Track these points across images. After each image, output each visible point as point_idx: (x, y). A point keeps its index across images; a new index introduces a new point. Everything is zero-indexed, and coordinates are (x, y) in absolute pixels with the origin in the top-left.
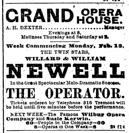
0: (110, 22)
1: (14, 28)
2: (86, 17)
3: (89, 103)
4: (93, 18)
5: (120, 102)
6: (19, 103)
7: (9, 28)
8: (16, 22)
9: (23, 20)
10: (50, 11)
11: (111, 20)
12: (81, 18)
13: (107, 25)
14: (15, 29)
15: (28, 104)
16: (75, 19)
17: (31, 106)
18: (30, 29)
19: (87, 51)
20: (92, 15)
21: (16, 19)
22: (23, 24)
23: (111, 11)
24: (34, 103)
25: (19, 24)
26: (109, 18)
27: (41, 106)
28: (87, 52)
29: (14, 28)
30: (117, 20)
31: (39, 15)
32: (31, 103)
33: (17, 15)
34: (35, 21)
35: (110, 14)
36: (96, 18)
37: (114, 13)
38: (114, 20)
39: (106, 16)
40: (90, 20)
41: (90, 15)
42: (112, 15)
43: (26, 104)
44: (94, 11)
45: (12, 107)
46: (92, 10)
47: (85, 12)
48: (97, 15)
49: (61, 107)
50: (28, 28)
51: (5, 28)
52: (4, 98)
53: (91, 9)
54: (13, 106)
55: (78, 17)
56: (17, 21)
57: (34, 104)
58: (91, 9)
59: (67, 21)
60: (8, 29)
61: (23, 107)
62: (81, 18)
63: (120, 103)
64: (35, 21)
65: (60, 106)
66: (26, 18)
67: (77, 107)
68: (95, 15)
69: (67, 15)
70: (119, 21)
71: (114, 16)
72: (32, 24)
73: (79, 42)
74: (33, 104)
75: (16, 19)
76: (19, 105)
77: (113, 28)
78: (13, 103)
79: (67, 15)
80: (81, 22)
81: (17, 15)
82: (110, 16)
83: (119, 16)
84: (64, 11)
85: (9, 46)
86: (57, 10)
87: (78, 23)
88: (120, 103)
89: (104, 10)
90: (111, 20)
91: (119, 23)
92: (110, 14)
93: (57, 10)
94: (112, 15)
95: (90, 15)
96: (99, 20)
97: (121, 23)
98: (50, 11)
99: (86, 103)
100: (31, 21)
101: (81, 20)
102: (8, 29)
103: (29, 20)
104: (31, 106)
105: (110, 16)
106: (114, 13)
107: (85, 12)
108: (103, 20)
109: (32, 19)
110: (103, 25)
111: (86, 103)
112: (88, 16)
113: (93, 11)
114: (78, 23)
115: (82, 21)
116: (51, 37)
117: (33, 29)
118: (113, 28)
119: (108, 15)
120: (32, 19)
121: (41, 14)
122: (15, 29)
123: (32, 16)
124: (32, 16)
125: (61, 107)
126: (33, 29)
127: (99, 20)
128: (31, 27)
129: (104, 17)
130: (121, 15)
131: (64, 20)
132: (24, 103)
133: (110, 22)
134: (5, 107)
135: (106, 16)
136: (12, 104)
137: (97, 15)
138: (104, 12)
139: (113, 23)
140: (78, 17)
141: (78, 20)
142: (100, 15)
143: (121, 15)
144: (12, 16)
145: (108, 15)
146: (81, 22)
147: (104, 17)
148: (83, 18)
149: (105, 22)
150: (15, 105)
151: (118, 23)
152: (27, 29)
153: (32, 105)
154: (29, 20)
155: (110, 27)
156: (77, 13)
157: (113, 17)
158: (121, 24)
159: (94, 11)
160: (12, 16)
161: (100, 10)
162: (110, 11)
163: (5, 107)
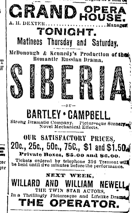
0: (112, 19)
1: (18, 23)
2: (88, 14)
3: (93, 162)
4: (95, 16)
5: (123, 162)
6: (24, 161)
7: (12, 23)
8: (20, 17)
9: (26, 17)
10: (53, 7)
11: (114, 17)
12: (84, 15)
13: (109, 22)
14: (19, 24)
15: (33, 162)
16: (78, 16)
17: (36, 164)
18: (33, 25)
19: (102, 191)
20: (95, 12)
21: (20, 15)
22: (26, 20)
23: (30, 8)
24: (39, 161)
25: (23, 19)
26: (112, 16)
27: (45, 164)
28: (103, 192)
29: (18, 24)
30: (120, 18)
31: (42, 12)
32: (36, 161)
33: (20, 11)
34: (38, 17)
35: (113, 12)
36: (99, 15)
37: (117, 11)
38: (117, 18)
39: (109, 13)
40: (93, 17)
41: (93, 12)
42: (115, 12)
43: (31, 162)
44: (97, 8)
45: (17, 164)
46: (95, 7)
47: (89, 9)
48: (100, 12)
49: (64, 165)
50: (31, 23)
51: (8, 23)
52: (9, 138)
53: (94, 7)
54: (19, 163)
55: (81, 14)
56: (21, 17)
57: (39, 162)
58: (94, 7)
59: (69, 17)
60: (12, 24)
61: (28, 165)
62: (84, 15)
63: (123, 163)
64: (38, 17)
65: (63, 164)
66: (29, 14)
67: (79, 166)
68: (97, 13)
69: (70, 12)
70: (122, 18)
71: (117, 14)
72: (35, 20)
73: (83, 132)
74: (38, 162)
75: (20, 15)
76: (24, 162)
77: (115, 26)
78: (18, 161)
79: (70, 12)
80: (83, 19)
81: (20, 11)
82: (113, 13)
83: (121, 13)
84: (67, 7)
85: (11, 52)
86: (60, 6)
87: (81, 19)
88: (123, 163)
89: (107, 7)
90: (114, 17)
91: (122, 21)
92: (113, 12)
93: (60, 6)
94: (115, 12)
95: (93, 12)
96: (102, 17)
97: (124, 20)
98: (53, 7)
99: (91, 162)
100: (34, 17)
101: (83, 17)
102: (12, 24)
103: (33, 16)
104: (36, 164)
105: (113, 13)
106: (117, 11)
107: (89, 9)
108: (106, 17)
109: (36, 15)
110: (106, 22)
111: (91, 162)
112: (91, 13)
113: (97, 8)
114: (81, 19)
115: (82, 15)
116: (61, 166)
117: (36, 25)
118: (115, 26)
119: (111, 12)
120: (36, 15)
121: (45, 9)
122: (19, 24)
123: (36, 12)
124: (36, 12)
125: (64, 165)
126: (36, 25)
127: (102, 17)
128: (33, 23)
129: (106, 14)
130: (125, 13)
131: (67, 17)
132: (29, 161)
133: (112, 19)
134: (8, 52)
135: (109, 13)
136: (17, 161)
137: (100, 12)
138: (107, 10)
139: (116, 20)
140: (81, 14)
141: (81, 17)
142: (103, 12)
143: (125, 13)
144: (16, 11)
145: (111, 12)
146: (83, 19)
147: (106, 14)
148: (86, 14)
149: (108, 19)
150: (21, 163)
151: (121, 21)
152: (30, 24)
153: (37, 163)
154: (33, 16)
155: (112, 25)
156: (80, 10)
157: (115, 15)
158: (124, 22)
159: (97, 8)
160: (16, 11)
161: (103, 7)
162: (113, 9)
163: (9, 121)
